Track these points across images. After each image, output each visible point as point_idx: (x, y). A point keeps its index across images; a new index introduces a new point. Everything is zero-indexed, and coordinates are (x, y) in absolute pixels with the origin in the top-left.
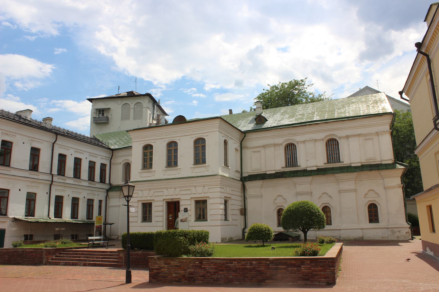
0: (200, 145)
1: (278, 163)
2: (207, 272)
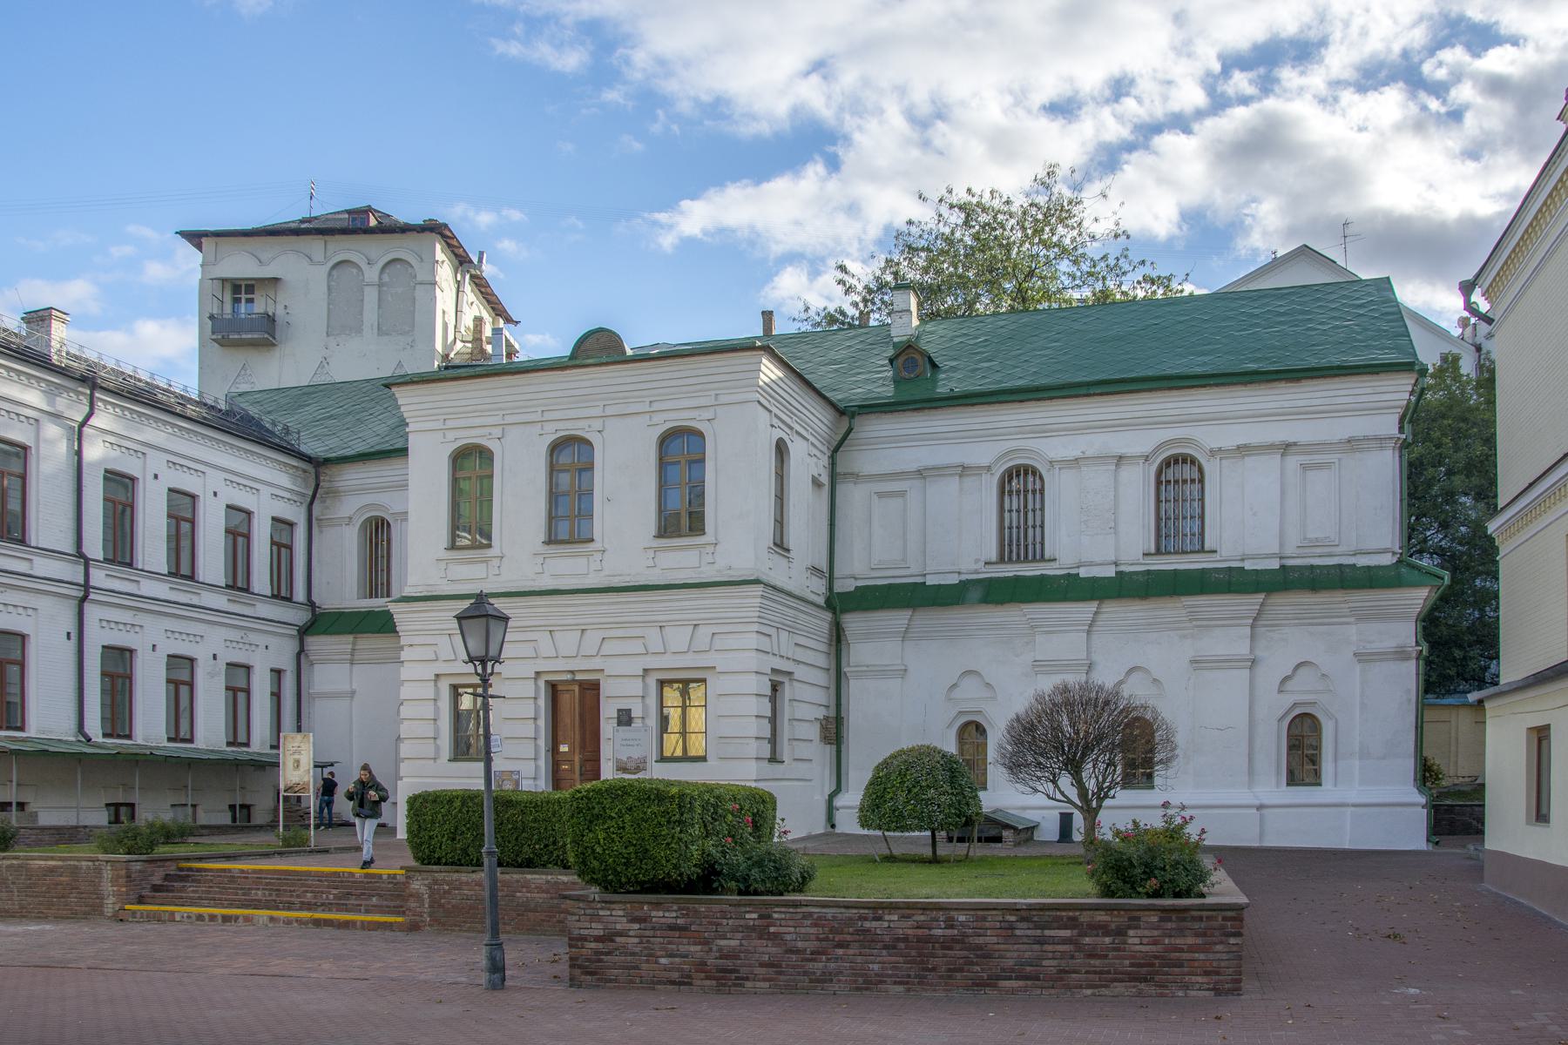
0: (680, 451)
1: (966, 541)
2: (790, 951)
